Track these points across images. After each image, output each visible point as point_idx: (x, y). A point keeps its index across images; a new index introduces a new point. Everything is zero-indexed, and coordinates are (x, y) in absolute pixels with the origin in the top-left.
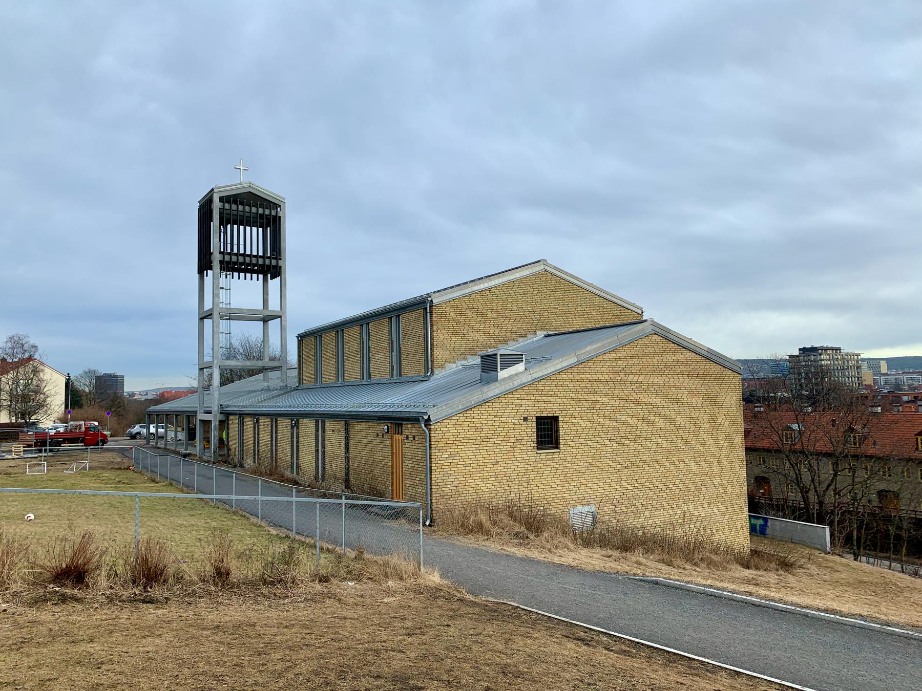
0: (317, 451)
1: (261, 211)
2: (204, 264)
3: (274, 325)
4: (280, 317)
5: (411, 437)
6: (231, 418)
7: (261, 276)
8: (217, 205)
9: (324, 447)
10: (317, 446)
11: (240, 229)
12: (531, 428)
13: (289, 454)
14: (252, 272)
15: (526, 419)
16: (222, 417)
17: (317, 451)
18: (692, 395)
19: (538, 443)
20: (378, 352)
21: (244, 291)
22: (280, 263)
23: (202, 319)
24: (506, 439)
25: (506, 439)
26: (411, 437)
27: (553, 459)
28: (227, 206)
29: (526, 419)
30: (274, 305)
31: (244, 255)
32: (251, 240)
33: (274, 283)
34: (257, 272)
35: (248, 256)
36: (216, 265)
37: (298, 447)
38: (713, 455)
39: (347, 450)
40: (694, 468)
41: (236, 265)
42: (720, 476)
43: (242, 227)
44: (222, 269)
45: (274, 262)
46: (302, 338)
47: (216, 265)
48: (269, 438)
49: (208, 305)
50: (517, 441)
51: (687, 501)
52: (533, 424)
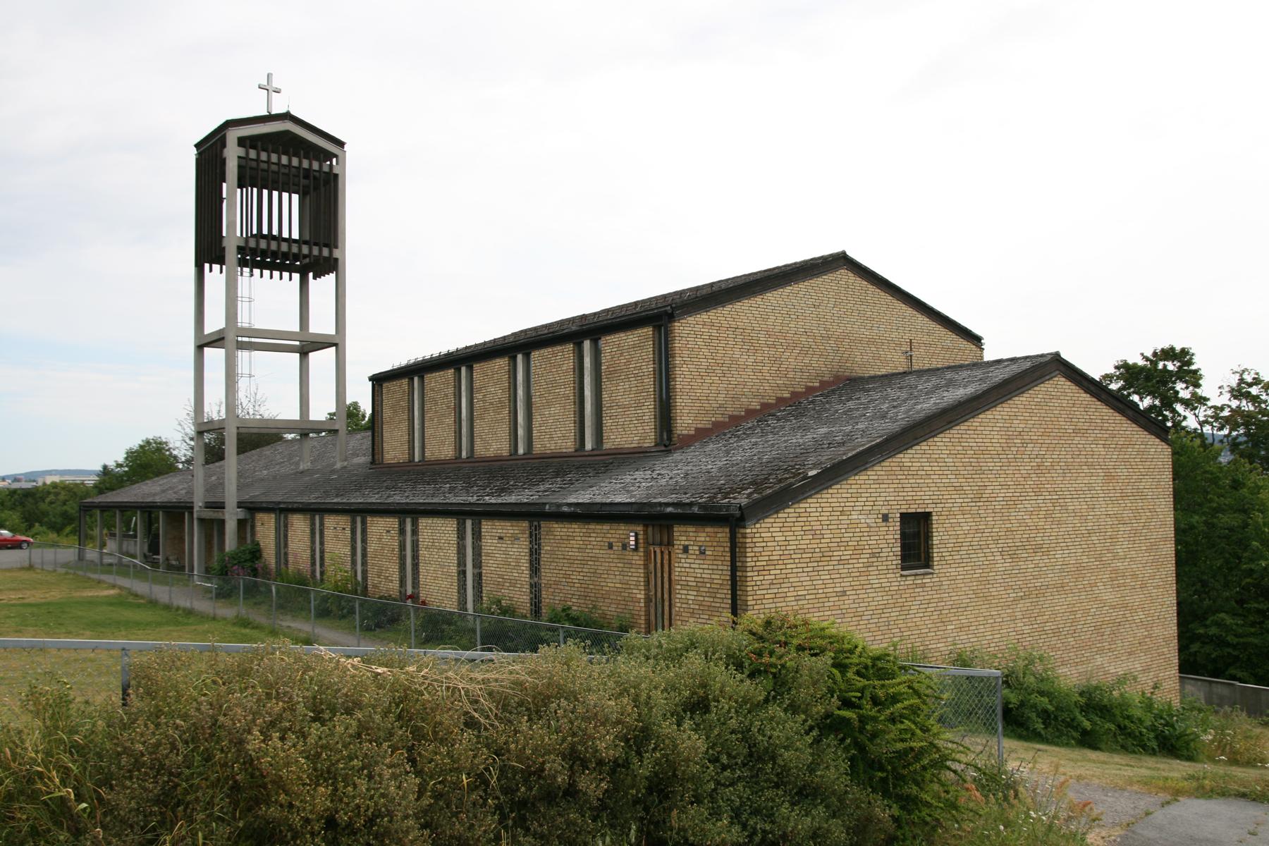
0: (462, 573)
1: (306, 164)
2: (209, 248)
3: (322, 360)
4: (336, 345)
5: (694, 549)
6: (260, 516)
7: (296, 276)
8: (232, 154)
9: (478, 564)
10: (461, 563)
11: (273, 188)
12: (892, 534)
13: (396, 577)
14: (282, 268)
15: (885, 518)
16: (241, 514)
17: (462, 573)
18: (1109, 477)
19: (904, 558)
20: (549, 404)
21: (270, 298)
22: (336, 253)
23: (200, 348)
24: (858, 550)
25: (858, 550)
26: (694, 549)
27: (923, 586)
28: (253, 154)
29: (885, 518)
30: (322, 324)
31: (270, 237)
32: (286, 215)
33: (322, 287)
34: (291, 270)
35: (285, 240)
36: (232, 255)
37: (416, 566)
38: (1134, 576)
39: (535, 568)
40: (1109, 596)
41: (265, 254)
42: (1143, 609)
43: (275, 194)
44: (243, 263)
45: (326, 252)
46: (379, 381)
47: (232, 255)
48: (348, 551)
49: (215, 322)
50: (873, 555)
51: (1100, 651)
52: (895, 526)
